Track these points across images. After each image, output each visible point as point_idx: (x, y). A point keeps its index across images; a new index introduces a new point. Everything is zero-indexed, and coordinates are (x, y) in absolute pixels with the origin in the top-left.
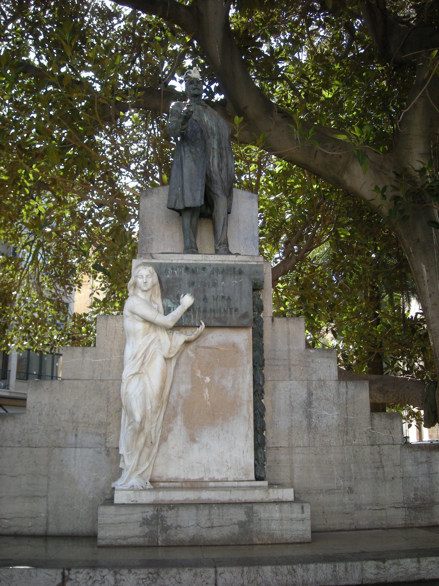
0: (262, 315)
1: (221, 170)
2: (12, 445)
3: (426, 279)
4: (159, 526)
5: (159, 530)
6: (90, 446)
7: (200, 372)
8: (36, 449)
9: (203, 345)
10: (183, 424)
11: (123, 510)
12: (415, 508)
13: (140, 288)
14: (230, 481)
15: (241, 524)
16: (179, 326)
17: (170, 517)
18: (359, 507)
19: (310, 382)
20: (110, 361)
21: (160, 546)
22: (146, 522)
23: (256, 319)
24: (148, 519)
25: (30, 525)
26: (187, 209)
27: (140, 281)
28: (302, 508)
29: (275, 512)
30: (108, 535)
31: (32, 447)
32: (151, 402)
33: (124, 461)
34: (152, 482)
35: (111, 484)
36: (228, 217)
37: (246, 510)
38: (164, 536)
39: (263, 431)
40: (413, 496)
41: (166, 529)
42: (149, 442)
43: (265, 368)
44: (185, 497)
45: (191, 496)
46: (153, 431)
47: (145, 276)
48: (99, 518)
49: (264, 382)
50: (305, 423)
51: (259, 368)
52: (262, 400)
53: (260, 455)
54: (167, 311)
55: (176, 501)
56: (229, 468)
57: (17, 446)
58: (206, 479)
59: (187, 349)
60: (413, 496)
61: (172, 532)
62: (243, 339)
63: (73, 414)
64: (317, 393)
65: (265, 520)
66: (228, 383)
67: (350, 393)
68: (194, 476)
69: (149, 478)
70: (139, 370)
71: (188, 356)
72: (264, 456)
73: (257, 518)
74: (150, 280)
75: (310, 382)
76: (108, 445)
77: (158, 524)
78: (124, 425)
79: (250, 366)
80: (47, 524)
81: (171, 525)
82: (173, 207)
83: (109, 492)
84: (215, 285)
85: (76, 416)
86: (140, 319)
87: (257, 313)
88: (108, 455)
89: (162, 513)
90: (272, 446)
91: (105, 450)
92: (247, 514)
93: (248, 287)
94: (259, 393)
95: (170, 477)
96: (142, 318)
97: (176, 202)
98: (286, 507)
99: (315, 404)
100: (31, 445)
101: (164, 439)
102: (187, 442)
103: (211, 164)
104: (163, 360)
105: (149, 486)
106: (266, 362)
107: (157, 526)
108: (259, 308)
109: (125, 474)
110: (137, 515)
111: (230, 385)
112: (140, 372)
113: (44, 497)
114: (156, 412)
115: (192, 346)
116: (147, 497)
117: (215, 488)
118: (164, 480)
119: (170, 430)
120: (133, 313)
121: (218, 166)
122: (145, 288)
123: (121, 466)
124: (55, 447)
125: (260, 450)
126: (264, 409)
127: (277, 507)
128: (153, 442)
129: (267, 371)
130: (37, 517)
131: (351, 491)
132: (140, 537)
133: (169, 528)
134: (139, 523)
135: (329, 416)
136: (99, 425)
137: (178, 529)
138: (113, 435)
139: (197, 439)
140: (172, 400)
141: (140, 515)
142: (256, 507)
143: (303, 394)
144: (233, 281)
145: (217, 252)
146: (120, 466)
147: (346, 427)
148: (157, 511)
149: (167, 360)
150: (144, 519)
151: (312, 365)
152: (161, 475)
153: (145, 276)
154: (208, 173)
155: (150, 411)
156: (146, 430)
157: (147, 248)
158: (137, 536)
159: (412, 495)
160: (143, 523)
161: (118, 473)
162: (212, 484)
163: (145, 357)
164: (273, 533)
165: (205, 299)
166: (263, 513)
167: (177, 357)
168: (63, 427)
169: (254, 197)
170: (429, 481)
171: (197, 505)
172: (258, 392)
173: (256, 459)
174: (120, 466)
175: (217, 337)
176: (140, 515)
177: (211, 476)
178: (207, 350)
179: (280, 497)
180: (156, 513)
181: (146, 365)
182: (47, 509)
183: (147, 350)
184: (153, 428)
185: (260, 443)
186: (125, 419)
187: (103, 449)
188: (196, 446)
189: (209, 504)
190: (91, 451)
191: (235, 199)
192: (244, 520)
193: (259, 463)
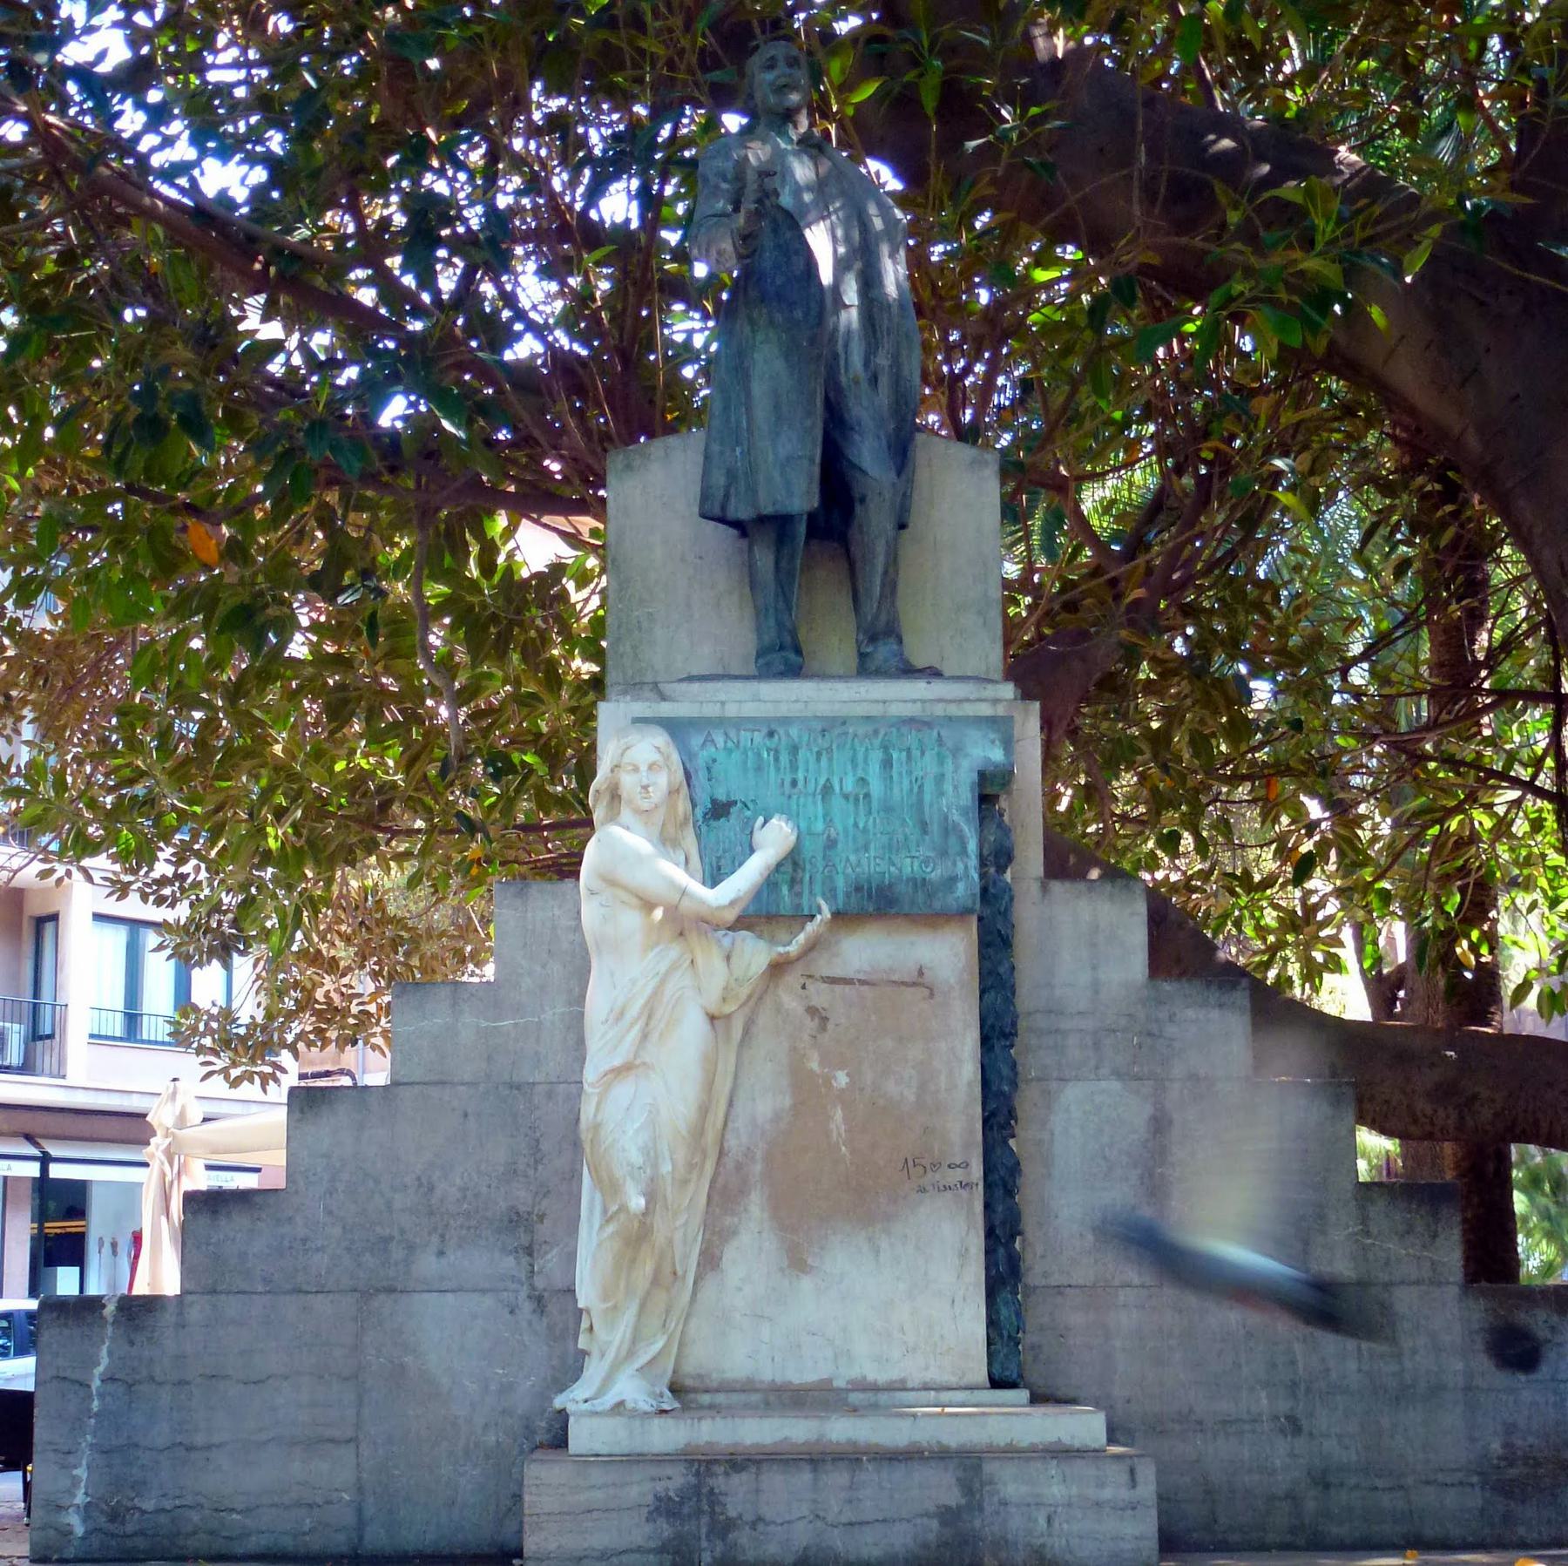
0: (1008, 876)
1: (874, 380)
2: (245, 1286)
4: (705, 1520)
5: (704, 1530)
6: (487, 1286)
7: (816, 1056)
8: (320, 1296)
9: (826, 972)
10: (766, 1215)
12: (1506, 1489)
13: (630, 802)
14: (913, 1389)
15: (948, 1516)
17: (736, 1493)
20: (540, 1023)
22: (664, 1508)
23: (992, 890)
24: (670, 1498)
25: (306, 1529)
26: (762, 520)
27: (628, 782)
28: (1132, 1472)
29: (1055, 1486)
30: (552, 1546)
31: (308, 1292)
32: (672, 1153)
33: (591, 1328)
34: (676, 1389)
35: (551, 1400)
36: (896, 539)
37: (960, 1473)
38: (719, 1548)
39: (1013, 1237)
40: (1500, 1451)
41: (723, 1528)
42: (667, 1270)
43: (1017, 1041)
44: (779, 1436)
45: (797, 1430)
46: (678, 1236)
47: (644, 768)
48: (527, 1498)
49: (1014, 1084)
51: (998, 1045)
52: (1012, 1142)
53: (1004, 1312)
54: (714, 878)
55: (752, 1445)
56: (910, 1350)
57: (260, 1289)
58: (839, 1383)
59: (776, 986)
60: (1500, 1451)
61: (742, 1537)
62: (948, 954)
63: (431, 1189)
65: (1017, 1506)
68: (805, 1373)
69: (666, 1381)
70: (636, 1056)
71: (778, 1009)
72: (1018, 1314)
73: (996, 1499)
74: (662, 781)
76: (540, 1283)
77: (699, 1512)
78: (590, 1220)
80: (361, 1524)
81: (740, 1517)
82: (717, 511)
83: (543, 1424)
85: (438, 1193)
86: (634, 901)
87: (992, 870)
89: (711, 1482)
90: (1044, 1282)
91: (529, 1297)
92: (968, 1489)
94: (1001, 1119)
95: (729, 1375)
96: (637, 896)
97: (727, 496)
98: (1080, 1467)
100: (305, 1287)
101: (710, 1260)
102: (782, 1270)
103: (842, 363)
104: (706, 1027)
105: (669, 1403)
106: (1022, 1024)
107: (698, 1519)
108: (998, 857)
109: (594, 1371)
110: (640, 1489)
112: (638, 1062)
113: (349, 1441)
114: (686, 1182)
115: (793, 979)
116: (669, 1435)
118: (715, 1385)
120: (611, 882)
121: (867, 364)
122: (645, 805)
123: (582, 1343)
124: (378, 1290)
125: (1004, 1295)
126: (1015, 1169)
127: (1053, 1468)
128: (680, 1273)
130: (328, 1502)
131: (1293, 1426)
132: (650, 1551)
134: (646, 1510)
136: (511, 1221)
137: (761, 1527)
138: (555, 1251)
139: (810, 1261)
140: (732, 1143)
141: (647, 1487)
145: (865, 669)
146: (580, 1346)
148: (698, 1474)
150: (658, 1498)
151: (1171, 1030)
152: (703, 1372)
153: (644, 768)
154: (832, 395)
155: (669, 1181)
156: (659, 1237)
157: (634, 647)
158: (639, 1550)
159: (1496, 1446)
160: (657, 1509)
161: (570, 1369)
162: (855, 1398)
163: (650, 1017)
164: (1043, 1546)
166: (1011, 1484)
167: (747, 1010)
168: (402, 1232)
169: (986, 463)
170: (1555, 1404)
171: (816, 1459)
172: (998, 1115)
173: (992, 1323)
174: (580, 1346)
176: (647, 1486)
177: (855, 1373)
178: (838, 988)
179: (1066, 1440)
180: (693, 1480)
181: (654, 1037)
182: (359, 1479)
183: (657, 993)
184: (681, 1232)
185: (1004, 1274)
186: (592, 1201)
187: (524, 1293)
188: (806, 1283)
189: (852, 1457)
190: (488, 1301)
191: (922, 475)
192: (953, 1504)
193: (1001, 1336)
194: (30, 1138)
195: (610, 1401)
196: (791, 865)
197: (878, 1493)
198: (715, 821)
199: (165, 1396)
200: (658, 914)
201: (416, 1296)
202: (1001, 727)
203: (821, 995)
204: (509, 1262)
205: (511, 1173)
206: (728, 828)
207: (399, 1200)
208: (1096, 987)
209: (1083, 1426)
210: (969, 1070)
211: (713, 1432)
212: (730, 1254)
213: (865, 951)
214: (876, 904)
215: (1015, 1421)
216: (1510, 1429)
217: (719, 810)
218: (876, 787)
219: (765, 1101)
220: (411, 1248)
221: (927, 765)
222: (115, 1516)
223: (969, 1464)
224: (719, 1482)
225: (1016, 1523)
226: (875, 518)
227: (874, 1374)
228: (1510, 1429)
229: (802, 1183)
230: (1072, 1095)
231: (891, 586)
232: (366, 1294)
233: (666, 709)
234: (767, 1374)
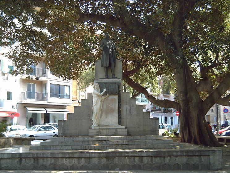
11: (93, 130)
15: (114, 132)
16: (103, 95)
17: (101, 131)
18: (140, 131)
19: (130, 105)
21: (35, 159)
29: (121, 130)
35: (34, 80)
45: (106, 127)
50: (129, 114)
61: (102, 134)
62: (116, 97)
68: (107, 124)
75: (130, 105)
84: (110, 86)
88: (90, 120)
93: (117, 86)
101: (101, 117)
109: (94, 124)
110: (96, 131)
116: (98, 128)
119: (102, 115)
142: (117, 129)
143: (129, 108)
144: (114, 85)
165: (109, 89)
166: (118, 130)
172: (119, 108)
175: (111, 97)
194: (44, 108)
195: (94, 125)
200: (141, 28)
201: (61, 157)
204: (88, 117)
205: (89, 112)
209: (124, 127)
212: (102, 117)
223: (116, 129)
226: (113, 65)
227: (111, 124)
233: (98, 81)
234: (105, 124)
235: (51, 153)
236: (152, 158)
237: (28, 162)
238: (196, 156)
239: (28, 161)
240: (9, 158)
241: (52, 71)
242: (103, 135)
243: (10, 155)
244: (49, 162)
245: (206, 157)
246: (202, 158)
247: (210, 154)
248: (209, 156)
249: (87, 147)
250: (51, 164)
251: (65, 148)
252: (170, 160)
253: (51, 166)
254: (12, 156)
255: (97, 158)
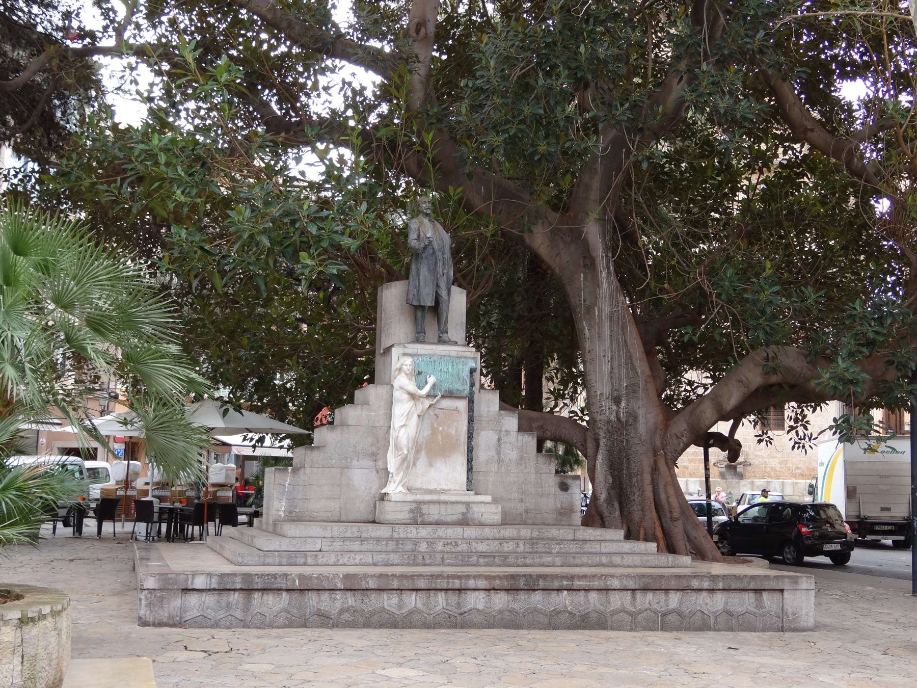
3: (607, 309)
12: (561, 514)
15: (463, 514)
17: (425, 509)
22: (412, 511)
29: (482, 509)
41: (422, 515)
45: (434, 497)
50: (496, 457)
61: (426, 517)
62: (462, 405)
64: (504, 439)
66: (453, 432)
67: (525, 440)
79: (466, 421)
99: (503, 446)
110: (407, 507)
111: (454, 432)
115: (432, 408)
116: (410, 498)
117: (453, 495)
120: (401, 388)
129: (476, 425)
131: (521, 501)
133: (424, 514)
135: (511, 454)
145: (441, 341)
147: (521, 460)
149: (419, 416)
171: (439, 502)
172: (470, 437)
185: (470, 470)
188: (433, 469)
189: (446, 503)
196: (434, 386)
197: (450, 509)
198: (418, 375)
199: (301, 488)
202: (474, 358)
203: (437, 411)
204: (371, 463)
205: (373, 445)
206: (422, 377)
207: (350, 449)
208: (489, 411)
210: (465, 428)
211: (419, 497)
213: (446, 403)
214: (450, 395)
215: (471, 497)
216: (562, 502)
217: (420, 373)
218: (450, 370)
219: (427, 433)
220: (352, 460)
221: (460, 366)
222: (290, 513)
223: (467, 504)
224: (422, 507)
225: (476, 516)
226: (443, 306)
228: (562, 502)
229: (431, 447)
230: (483, 433)
231: (446, 322)
232: (343, 468)
235: (347, 577)
236: (634, 597)
237: (270, 603)
238: (235, 590)
239: (270, 598)
240: (210, 590)
241: (476, 337)
242: (431, 520)
243: (213, 580)
244: (338, 605)
245: (777, 596)
246: (765, 596)
247: (785, 587)
248: (782, 591)
249: (420, 558)
250: (342, 611)
251: (351, 560)
252: (681, 602)
253: (342, 617)
254: (220, 584)
255: (482, 593)
